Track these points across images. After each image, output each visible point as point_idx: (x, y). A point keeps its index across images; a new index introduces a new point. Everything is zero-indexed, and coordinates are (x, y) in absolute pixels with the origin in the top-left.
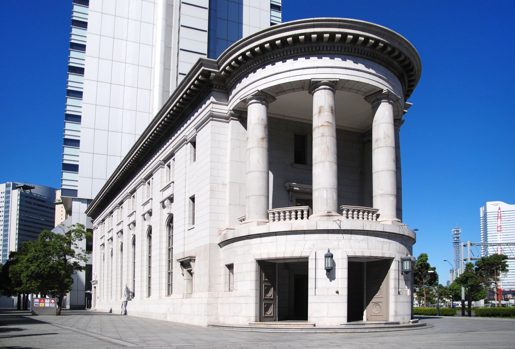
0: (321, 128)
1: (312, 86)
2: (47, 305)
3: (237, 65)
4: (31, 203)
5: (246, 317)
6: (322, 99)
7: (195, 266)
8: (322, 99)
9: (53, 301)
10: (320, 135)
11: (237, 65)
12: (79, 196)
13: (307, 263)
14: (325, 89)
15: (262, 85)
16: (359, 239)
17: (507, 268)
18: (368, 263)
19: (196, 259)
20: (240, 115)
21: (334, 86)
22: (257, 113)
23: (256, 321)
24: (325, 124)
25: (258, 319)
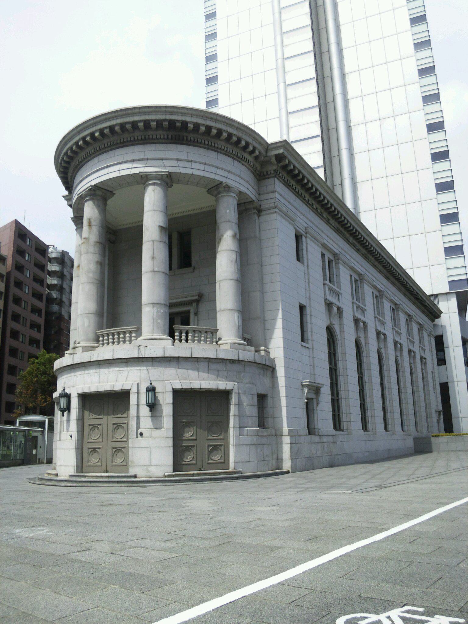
3: (77, 150)
6: (152, 197)
8: (152, 197)
11: (77, 150)
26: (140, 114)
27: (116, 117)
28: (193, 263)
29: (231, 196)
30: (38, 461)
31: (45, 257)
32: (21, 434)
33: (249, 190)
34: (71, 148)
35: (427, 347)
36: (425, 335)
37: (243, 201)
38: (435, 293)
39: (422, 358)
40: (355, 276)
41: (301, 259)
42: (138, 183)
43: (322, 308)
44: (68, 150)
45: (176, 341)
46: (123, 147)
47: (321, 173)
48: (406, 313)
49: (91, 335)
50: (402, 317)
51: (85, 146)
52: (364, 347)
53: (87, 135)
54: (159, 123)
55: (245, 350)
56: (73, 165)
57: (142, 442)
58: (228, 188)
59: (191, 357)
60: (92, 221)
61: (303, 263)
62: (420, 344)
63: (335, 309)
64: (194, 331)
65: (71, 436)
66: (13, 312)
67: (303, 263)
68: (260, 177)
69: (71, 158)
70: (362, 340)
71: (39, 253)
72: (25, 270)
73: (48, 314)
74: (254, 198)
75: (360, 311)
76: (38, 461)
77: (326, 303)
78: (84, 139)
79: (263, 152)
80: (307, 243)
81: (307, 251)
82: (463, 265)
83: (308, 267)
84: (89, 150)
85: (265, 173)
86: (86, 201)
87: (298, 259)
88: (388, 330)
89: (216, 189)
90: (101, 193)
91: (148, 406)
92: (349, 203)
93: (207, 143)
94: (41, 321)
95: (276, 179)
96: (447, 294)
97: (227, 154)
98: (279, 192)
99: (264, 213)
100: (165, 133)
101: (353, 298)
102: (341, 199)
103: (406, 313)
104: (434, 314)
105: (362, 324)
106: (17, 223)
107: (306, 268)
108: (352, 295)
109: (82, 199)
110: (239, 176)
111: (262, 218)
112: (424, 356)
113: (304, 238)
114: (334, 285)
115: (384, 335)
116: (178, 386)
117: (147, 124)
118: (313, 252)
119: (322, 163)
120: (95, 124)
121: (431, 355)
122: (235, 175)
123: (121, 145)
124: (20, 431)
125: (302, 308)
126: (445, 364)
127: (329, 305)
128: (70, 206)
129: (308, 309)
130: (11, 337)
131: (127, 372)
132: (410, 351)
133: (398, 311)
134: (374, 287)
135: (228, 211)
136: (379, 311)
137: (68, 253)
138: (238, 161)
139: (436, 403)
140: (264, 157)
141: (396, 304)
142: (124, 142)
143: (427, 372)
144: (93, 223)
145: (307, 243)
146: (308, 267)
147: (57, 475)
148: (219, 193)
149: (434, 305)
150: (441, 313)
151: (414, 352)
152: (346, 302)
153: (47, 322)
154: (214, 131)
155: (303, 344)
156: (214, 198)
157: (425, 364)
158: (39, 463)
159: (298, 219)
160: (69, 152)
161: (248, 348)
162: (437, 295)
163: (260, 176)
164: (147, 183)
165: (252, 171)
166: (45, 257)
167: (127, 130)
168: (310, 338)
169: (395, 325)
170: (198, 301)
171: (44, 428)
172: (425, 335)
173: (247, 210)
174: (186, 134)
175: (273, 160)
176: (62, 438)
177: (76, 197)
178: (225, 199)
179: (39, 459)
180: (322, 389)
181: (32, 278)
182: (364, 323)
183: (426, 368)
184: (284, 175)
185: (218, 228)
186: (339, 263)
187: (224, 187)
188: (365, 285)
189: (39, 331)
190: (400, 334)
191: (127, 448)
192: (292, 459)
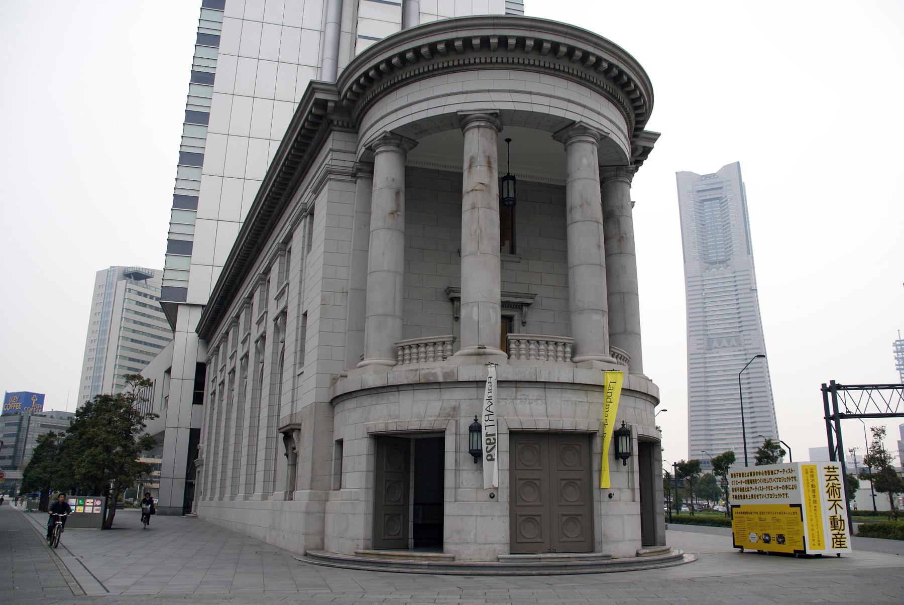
0: (471, 193)
1: (460, 122)
2: (88, 510)
3: (360, 91)
4: (144, 305)
5: (353, 540)
6: (478, 145)
7: (851, 448)
8: (478, 145)
9: (98, 503)
10: (470, 207)
11: (360, 91)
12: (189, 300)
13: (442, 440)
14: (479, 127)
15: (392, 124)
16: (530, 397)
17: (758, 455)
18: (417, 440)
19: (302, 427)
20: (365, 169)
21: (496, 120)
22: (387, 167)
23: (367, 548)
24: (477, 188)
25: (370, 545)
42: (452, 126)
44: (353, 84)
45: (513, 357)
51: (318, 121)
58: (584, 130)
64: (538, 342)
69: (357, 95)
89: (565, 132)
91: (472, 454)
93: (552, 66)
135: (585, 162)
142: (434, 70)
156: (561, 145)
160: (354, 87)
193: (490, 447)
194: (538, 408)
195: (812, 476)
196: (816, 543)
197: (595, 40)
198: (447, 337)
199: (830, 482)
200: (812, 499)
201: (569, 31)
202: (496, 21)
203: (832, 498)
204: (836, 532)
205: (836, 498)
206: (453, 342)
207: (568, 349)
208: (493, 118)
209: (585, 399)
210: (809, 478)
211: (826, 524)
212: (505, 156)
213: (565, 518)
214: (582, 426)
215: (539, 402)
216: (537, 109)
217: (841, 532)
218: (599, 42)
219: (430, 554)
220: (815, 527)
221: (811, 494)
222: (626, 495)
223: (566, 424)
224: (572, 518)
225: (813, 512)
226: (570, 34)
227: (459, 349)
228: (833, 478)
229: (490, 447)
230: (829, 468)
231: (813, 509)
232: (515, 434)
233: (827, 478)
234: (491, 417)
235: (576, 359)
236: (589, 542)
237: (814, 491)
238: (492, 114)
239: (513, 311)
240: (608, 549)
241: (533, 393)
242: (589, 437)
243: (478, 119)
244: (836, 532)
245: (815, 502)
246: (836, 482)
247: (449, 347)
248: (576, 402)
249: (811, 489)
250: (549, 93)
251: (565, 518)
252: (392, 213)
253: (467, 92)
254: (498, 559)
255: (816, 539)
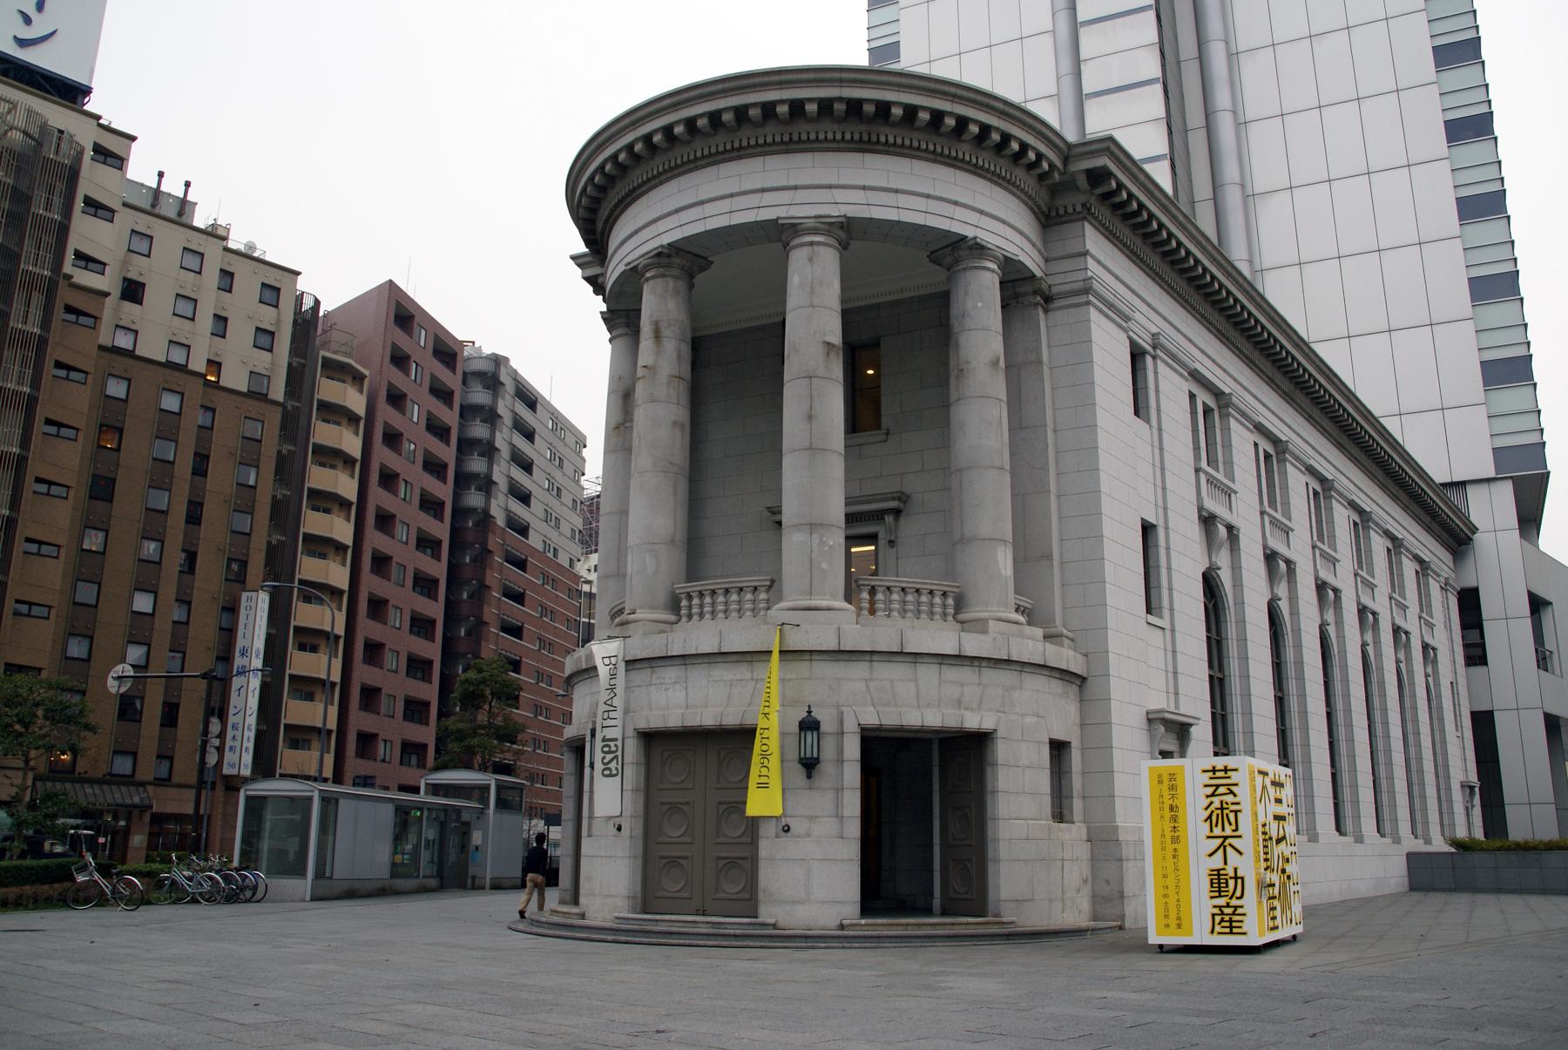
1: (781, 234)
26: (782, 85)
27: (725, 93)
28: (886, 422)
29: (988, 269)
30: (470, 881)
31: (453, 370)
32: (39, 784)
33: (1029, 257)
34: (615, 157)
35: (1438, 617)
36: (1434, 587)
37: (1014, 277)
38: (1456, 479)
39: (1426, 647)
40: (1265, 445)
41: (1141, 412)
43: (1194, 530)
46: (740, 158)
47: (1161, 175)
48: (1388, 534)
49: (662, 597)
50: (1342, 517)
52: (1230, 596)
53: (655, 131)
54: (826, 106)
55: (1022, 636)
56: (614, 196)
57: (790, 848)
58: (979, 249)
59: (901, 653)
60: (663, 326)
61: (1148, 421)
62: (1393, 590)
63: (1222, 531)
65: (619, 829)
66: (378, 508)
67: (1148, 421)
68: (1049, 219)
70: (1225, 576)
71: (441, 361)
72: (409, 404)
73: (459, 512)
74: (1038, 273)
75: (1278, 533)
76: (470, 881)
77: (1200, 517)
78: (647, 138)
79: (1058, 163)
80: (1156, 373)
81: (1157, 391)
82: (1531, 407)
83: (1160, 429)
84: (659, 163)
85: (1062, 212)
86: (647, 280)
87: (1137, 413)
88: (1299, 548)
89: (953, 252)
90: (685, 260)
92: (1206, 222)
94: (441, 530)
95: (1086, 224)
96: (1488, 480)
97: (976, 170)
98: (1103, 260)
99: (1057, 304)
100: (836, 127)
101: (1197, 458)
102: (1214, 239)
103: (1388, 534)
104: (1457, 538)
105: (1282, 565)
106: (391, 289)
107: (1155, 431)
108: (1196, 448)
109: (634, 276)
110: (1004, 222)
111: (1058, 316)
112: (1330, 579)
113: (1149, 359)
114: (1217, 470)
115: (1335, 590)
116: (871, 719)
117: (797, 107)
118: (1170, 389)
119: (1163, 148)
120: (675, 106)
121: (1447, 638)
122: (994, 218)
123: (735, 154)
124: (431, 808)
125: (1147, 529)
126: (1486, 663)
127: (1208, 521)
128: (598, 288)
129: (1161, 532)
130: (372, 571)
131: (750, 686)
132: (1397, 630)
133: (1328, 498)
134: (1311, 471)
136: (1322, 529)
137: (507, 360)
138: (1000, 186)
139: (1463, 765)
140: (1061, 174)
141: (1322, 480)
143: (1437, 684)
144: (666, 332)
145: (1156, 373)
146: (1160, 429)
147: (583, 916)
148: (957, 262)
149: (1457, 511)
150: (1474, 530)
151: (1407, 633)
152: (1245, 512)
153: (455, 532)
154: (950, 122)
155: (1151, 619)
157: (1435, 661)
158: (474, 888)
159: (1137, 316)
161: (1028, 630)
162: (1463, 484)
163: (1048, 217)
164: (793, 243)
165: (1031, 209)
166: (453, 370)
167: (749, 120)
168: (1166, 603)
169: (1321, 537)
170: (897, 512)
171: (485, 802)
172: (1434, 587)
173: (1017, 296)
174: (886, 130)
175: (1082, 182)
176: (594, 831)
177: (621, 268)
178: (970, 275)
179: (474, 878)
180: (1193, 729)
181: (424, 422)
182: (1288, 562)
183: (1436, 673)
184: (1104, 212)
185: (957, 346)
186: (1285, 460)
187: (970, 248)
188: (1232, 421)
189: (437, 556)
190: (1334, 562)
191: (754, 860)
192: (1122, 896)
193: (609, 757)
194: (677, 695)
195: (1172, 788)
196: (1173, 922)
197: (776, 78)
198: (760, 579)
199: (1216, 801)
200: (1169, 834)
201: (727, 85)
202: (632, 118)
203: (1217, 831)
204: (1222, 901)
205: (1228, 831)
206: (770, 587)
207: (950, 601)
208: (664, 260)
209: (749, 675)
210: (1166, 793)
211: (1199, 886)
212: (694, 314)
213: (663, 862)
214: (731, 719)
215: (678, 687)
216: (712, 224)
217: (1234, 902)
218: (783, 77)
219: (911, 921)
220: (1172, 892)
221: (1168, 826)
222: (827, 826)
223: (707, 718)
224: (732, 863)
225: (1170, 862)
226: (731, 90)
227: (780, 599)
228: (1222, 790)
229: (609, 757)
230: (1214, 770)
231: (1169, 853)
232: (650, 739)
233: (1210, 790)
234: (612, 715)
235: (961, 617)
236: (748, 902)
237: (1174, 819)
238: (659, 255)
239: (867, 521)
240: (767, 914)
241: (671, 673)
242: (744, 736)
243: (647, 268)
244: (1222, 901)
245: (1175, 840)
246: (1230, 798)
247: (763, 596)
248: (731, 683)
249: (1167, 814)
250: (759, 186)
251: (663, 862)
252: (617, 428)
253: (796, 188)
254: (842, 927)
255: (1173, 913)
